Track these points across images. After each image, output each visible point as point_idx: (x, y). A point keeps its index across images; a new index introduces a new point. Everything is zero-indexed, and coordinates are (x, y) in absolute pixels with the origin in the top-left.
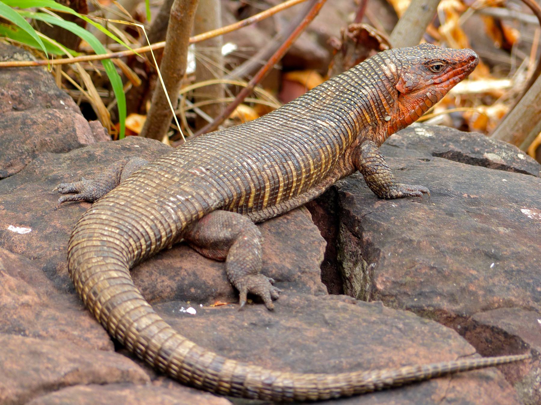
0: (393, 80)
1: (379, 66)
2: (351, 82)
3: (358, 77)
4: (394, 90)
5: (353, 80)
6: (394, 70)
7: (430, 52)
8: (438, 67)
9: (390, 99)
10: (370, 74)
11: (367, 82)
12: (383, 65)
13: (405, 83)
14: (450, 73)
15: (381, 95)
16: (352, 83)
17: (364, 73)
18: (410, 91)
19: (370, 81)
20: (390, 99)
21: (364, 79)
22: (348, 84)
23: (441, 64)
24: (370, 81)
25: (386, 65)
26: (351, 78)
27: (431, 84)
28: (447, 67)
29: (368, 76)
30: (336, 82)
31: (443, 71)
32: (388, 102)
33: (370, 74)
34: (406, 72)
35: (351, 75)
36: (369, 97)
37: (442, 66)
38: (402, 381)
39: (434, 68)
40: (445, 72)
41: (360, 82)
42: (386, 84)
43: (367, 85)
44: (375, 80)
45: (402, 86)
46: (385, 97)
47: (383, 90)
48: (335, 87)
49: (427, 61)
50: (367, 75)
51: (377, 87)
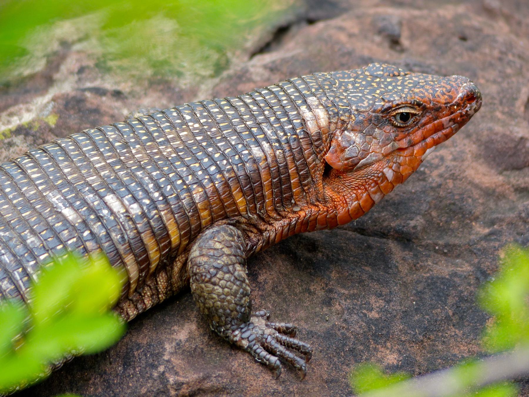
0: (320, 141)
1: (296, 108)
2: (239, 124)
3: (253, 117)
4: (318, 162)
5: (242, 121)
6: (323, 122)
7: (390, 83)
8: (405, 117)
9: (306, 176)
10: (278, 120)
11: (269, 132)
12: (303, 108)
13: (343, 150)
14: (429, 126)
15: (290, 165)
16: (240, 127)
17: (266, 113)
18: (352, 167)
19: (276, 133)
20: (306, 176)
21: (264, 126)
22: (231, 125)
23: (413, 111)
24: (276, 133)
25: (310, 108)
26: (240, 116)
27: (393, 152)
28: (423, 116)
29: (274, 121)
30: (211, 115)
31: (416, 123)
32: (300, 181)
33: (278, 120)
34: (346, 129)
35: (243, 109)
36: (262, 164)
37: (414, 115)
38: (198, 237)
39: (398, 117)
40: (419, 125)
41: (254, 130)
42: (305, 147)
43: (267, 139)
44: (285, 134)
45: (338, 157)
46: (298, 170)
47: (297, 156)
48: (201, 125)
49: (387, 105)
50: (272, 119)
51: (285, 146)
